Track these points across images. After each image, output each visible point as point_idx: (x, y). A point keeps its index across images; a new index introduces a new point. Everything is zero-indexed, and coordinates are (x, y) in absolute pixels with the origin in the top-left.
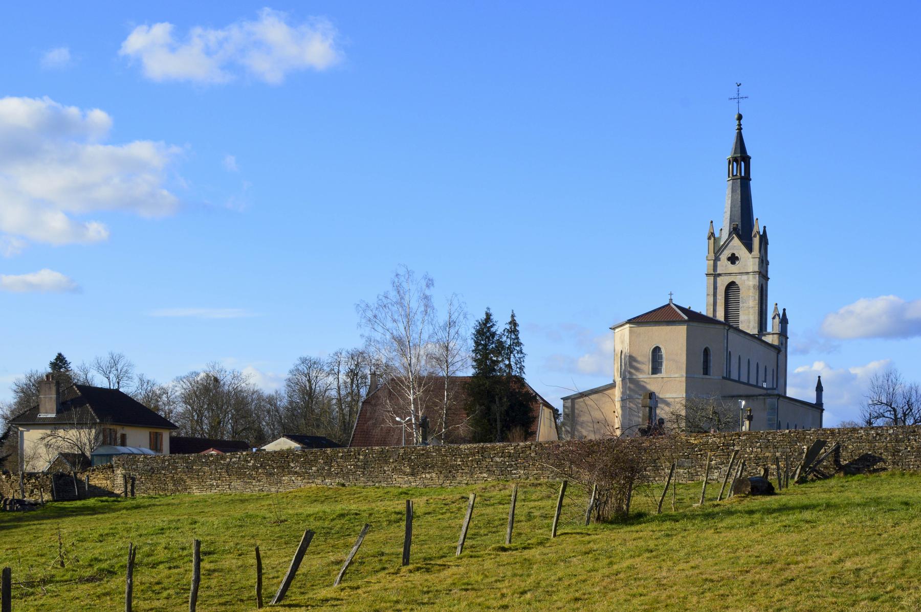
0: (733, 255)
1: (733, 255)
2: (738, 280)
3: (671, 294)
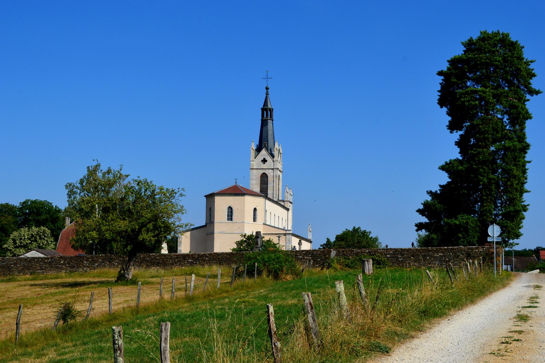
0: (264, 159)
1: (264, 159)
2: (267, 172)
3: (236, 180)
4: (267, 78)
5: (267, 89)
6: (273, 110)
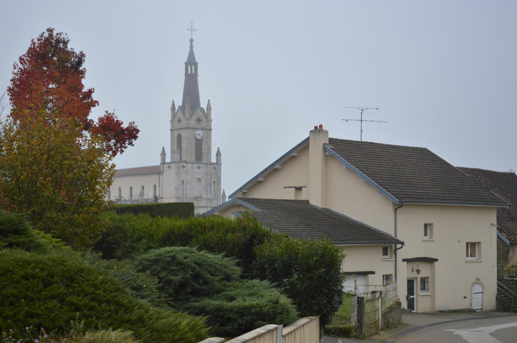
1: (199, 118)
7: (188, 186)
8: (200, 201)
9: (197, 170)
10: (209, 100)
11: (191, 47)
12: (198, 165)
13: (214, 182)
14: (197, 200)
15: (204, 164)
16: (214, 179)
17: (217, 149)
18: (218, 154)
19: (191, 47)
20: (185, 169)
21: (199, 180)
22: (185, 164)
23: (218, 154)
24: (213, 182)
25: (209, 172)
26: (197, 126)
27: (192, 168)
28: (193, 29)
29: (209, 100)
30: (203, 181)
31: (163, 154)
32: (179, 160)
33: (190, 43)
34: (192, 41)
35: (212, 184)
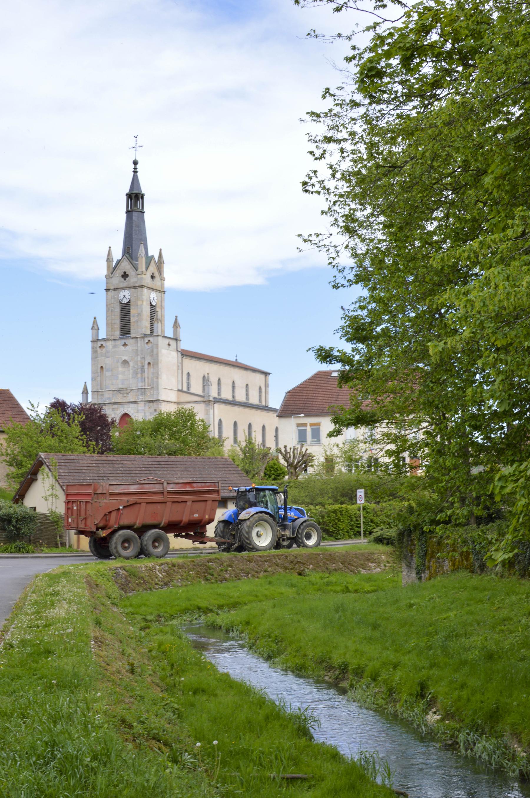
1: (125, 273)
4: (136, 147)
5: (135, 163)
6: (145, 197)
7: (108, 374)
8: (128, 394)
9: (123, 348)
10: (161, 250)
11: (135, 172)
12: (122, 342)
13: (149, 363)
14: (122, 392)
15: (132, 338)
16: (148, 359)
17: (93, 319)
18: (176, 325)
19: (135, 172)
20: (104, 350)
21: (125, 362)
22: (103, 343)
23: (176, 325)
24: (146, 363)
25: (139, 349)
26: (121, 285)
27: (115, 346)
28: (134, 146)
29: (161, 250)
30: (131, 364)
31: (95, 327)
32: (148, 332)
33: (133, 166)
34: (135, 163)
35: (146, 366)
